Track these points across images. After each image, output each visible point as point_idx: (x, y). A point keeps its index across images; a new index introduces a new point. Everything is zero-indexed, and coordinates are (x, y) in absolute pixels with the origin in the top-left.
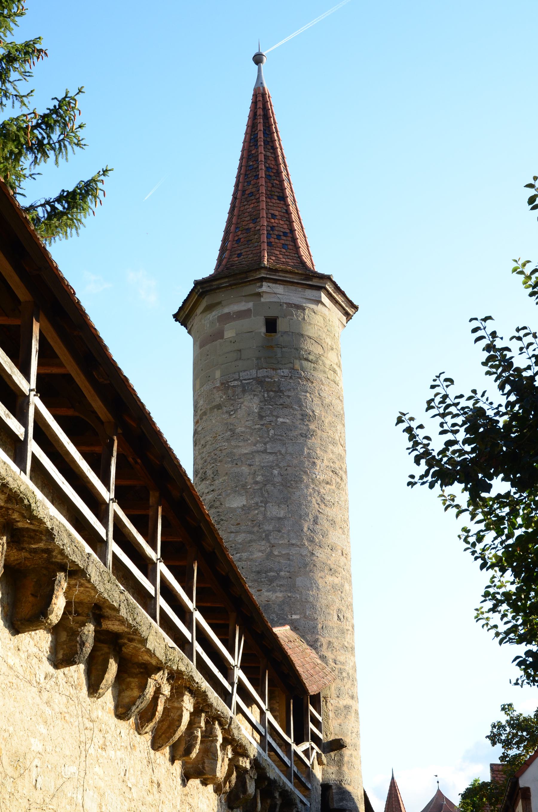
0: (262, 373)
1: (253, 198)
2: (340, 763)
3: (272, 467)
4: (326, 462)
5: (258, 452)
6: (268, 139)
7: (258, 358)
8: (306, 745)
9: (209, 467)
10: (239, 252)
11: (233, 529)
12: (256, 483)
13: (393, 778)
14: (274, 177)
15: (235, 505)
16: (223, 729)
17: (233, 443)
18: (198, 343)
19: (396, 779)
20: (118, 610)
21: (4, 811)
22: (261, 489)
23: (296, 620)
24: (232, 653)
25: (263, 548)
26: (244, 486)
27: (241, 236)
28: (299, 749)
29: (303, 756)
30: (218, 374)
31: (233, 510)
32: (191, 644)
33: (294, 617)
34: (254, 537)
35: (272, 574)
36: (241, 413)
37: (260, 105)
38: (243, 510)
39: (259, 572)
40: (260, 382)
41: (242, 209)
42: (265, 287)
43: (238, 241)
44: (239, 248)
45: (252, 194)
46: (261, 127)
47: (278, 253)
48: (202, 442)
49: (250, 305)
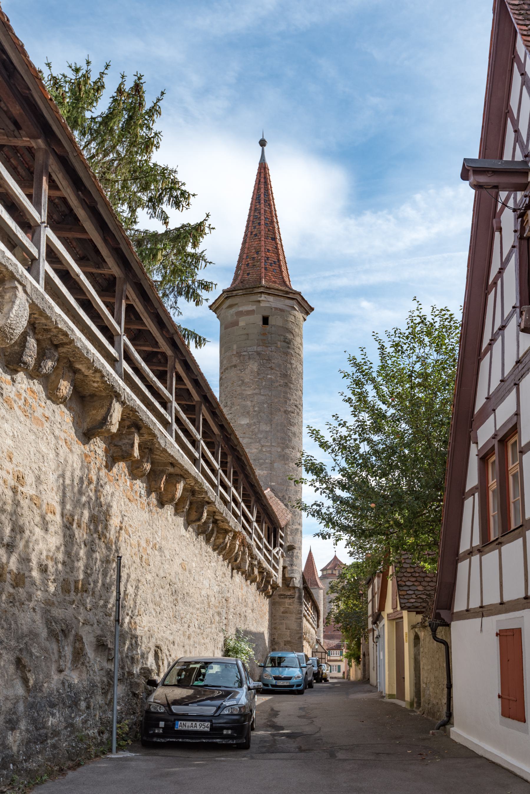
0: (259, 349)
1: (257, 237)
2: (292, 557)
3: (264, 403)
4: (292, 401)
5: (256, 394)
6: (267, 199)
8: (277, 549)
9: (229, 400)
10: (248, 272)
12: (255, 411)
13: (310, 551)
14: (270, 225)
15: (243, 423)
16: (249, 550)
17: (243, 388)
18: (223, 326)
19: (312, 551)
20: (222, 514)
22: (257, 415)
23: (273, 485)
24: (253, 516)
25: (257, 447)
26: (248, 413)
27: (250, 262)
28: (274, 552)
29: (276, 555)
30: (235, 347)
32: (240, 517)
33: (273, 484)
34: (253, 441)
35: (262, 461)
36: (248, 371)
37: (262, 175)
38: (247, 426)
40: (259, 354)
41: (250, 244)
42: (263, 297)
43: (248, 265)
44: (249, 269)
45: (256, 235)
46: (262, 190)
47: (270, 275)
48: (225, 385)
49: (254, 307)
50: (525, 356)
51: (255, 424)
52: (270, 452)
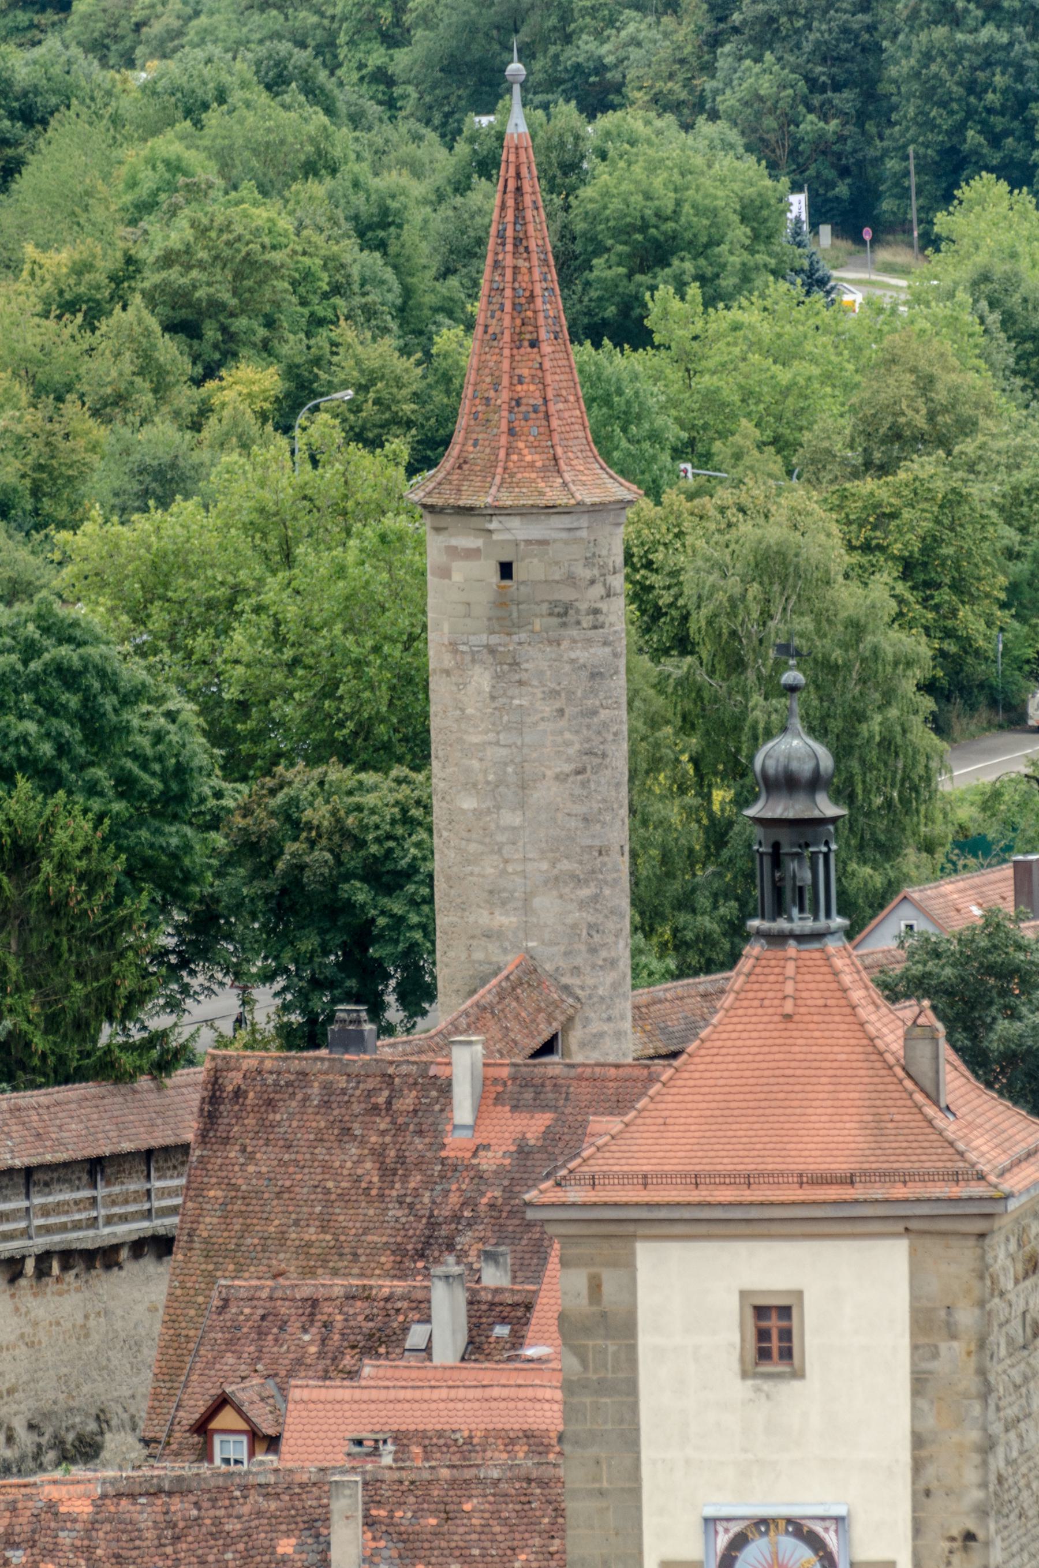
0: (494, 640)
3: (506, 764)
7: (489, 619)
11: (464, 834)
12: (488, 783)
15: (465, 806)
21: (1034, 435)
26: (475, 785)
31: (464, 812)
35: (505, 895)
39: (491, 892)
40: (492, 651)
46: (510, 217)
50: (62, 1172)
51: (489, 811)
52: (523, 874)
